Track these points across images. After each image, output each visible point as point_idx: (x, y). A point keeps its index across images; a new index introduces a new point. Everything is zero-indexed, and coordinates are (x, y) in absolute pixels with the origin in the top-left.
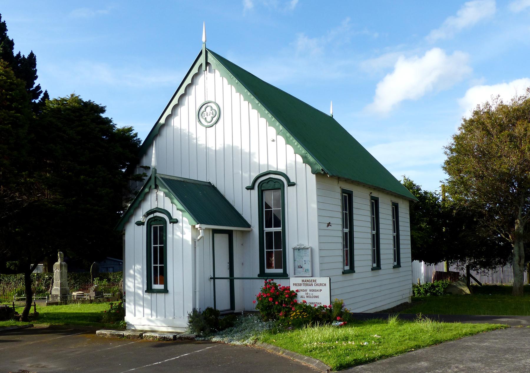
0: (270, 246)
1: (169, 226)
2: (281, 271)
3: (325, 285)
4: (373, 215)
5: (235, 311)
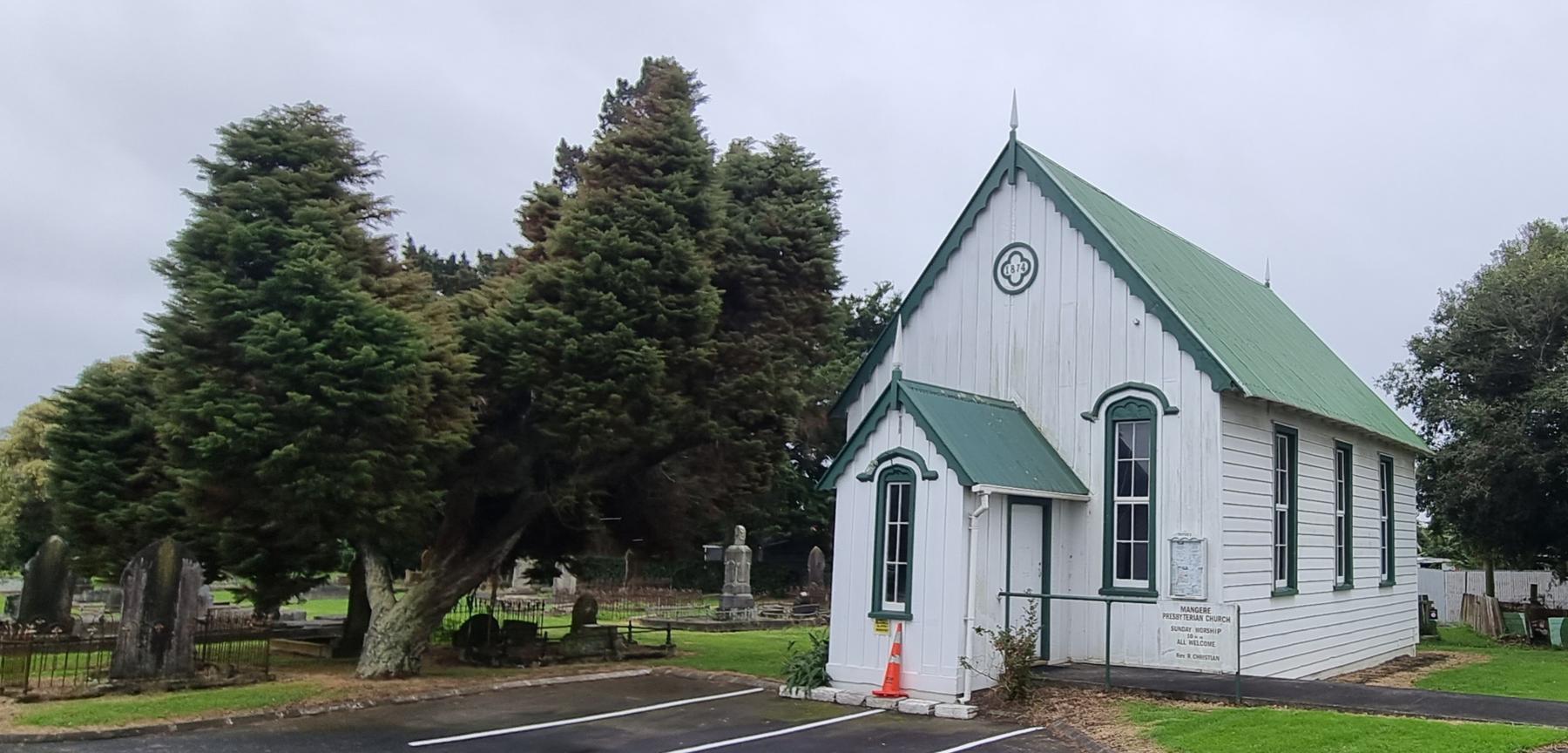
0: (1124, 533)
1: (922, 486)
2: (1143, 584)
5: (1050, 663)
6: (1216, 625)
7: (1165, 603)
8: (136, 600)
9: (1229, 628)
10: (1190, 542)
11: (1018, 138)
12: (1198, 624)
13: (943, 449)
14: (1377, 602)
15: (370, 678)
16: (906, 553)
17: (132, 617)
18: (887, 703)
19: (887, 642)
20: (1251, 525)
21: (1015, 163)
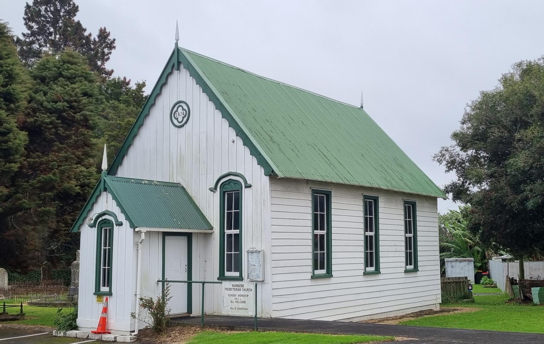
1: (116, 228)
2: (237, 274)
3: (251, 290)
4: (410, 218)
5: (191, 315)
7: (246, 283)
9: (252, 294)
10: (256, 252)
11: (180, 45)
13: (123, 211)
14: (403, 281)
16: (110, 264)
18: (97, 337)
19: (101, 306)
20: (342, 243)
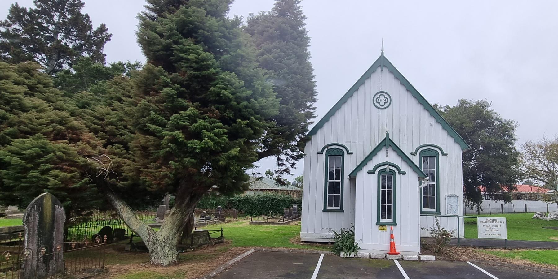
6: (499, 224)
8: (34, 231)
12: (493, 224)
15: (169, 265)
17: (33, 242)
21: (382, 64)
